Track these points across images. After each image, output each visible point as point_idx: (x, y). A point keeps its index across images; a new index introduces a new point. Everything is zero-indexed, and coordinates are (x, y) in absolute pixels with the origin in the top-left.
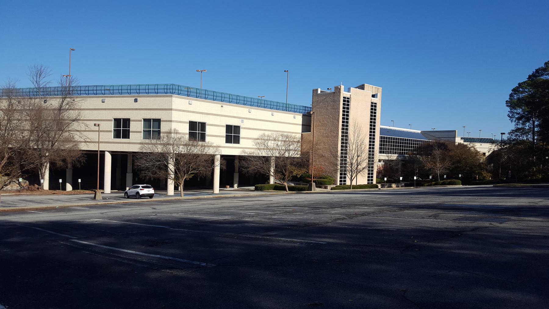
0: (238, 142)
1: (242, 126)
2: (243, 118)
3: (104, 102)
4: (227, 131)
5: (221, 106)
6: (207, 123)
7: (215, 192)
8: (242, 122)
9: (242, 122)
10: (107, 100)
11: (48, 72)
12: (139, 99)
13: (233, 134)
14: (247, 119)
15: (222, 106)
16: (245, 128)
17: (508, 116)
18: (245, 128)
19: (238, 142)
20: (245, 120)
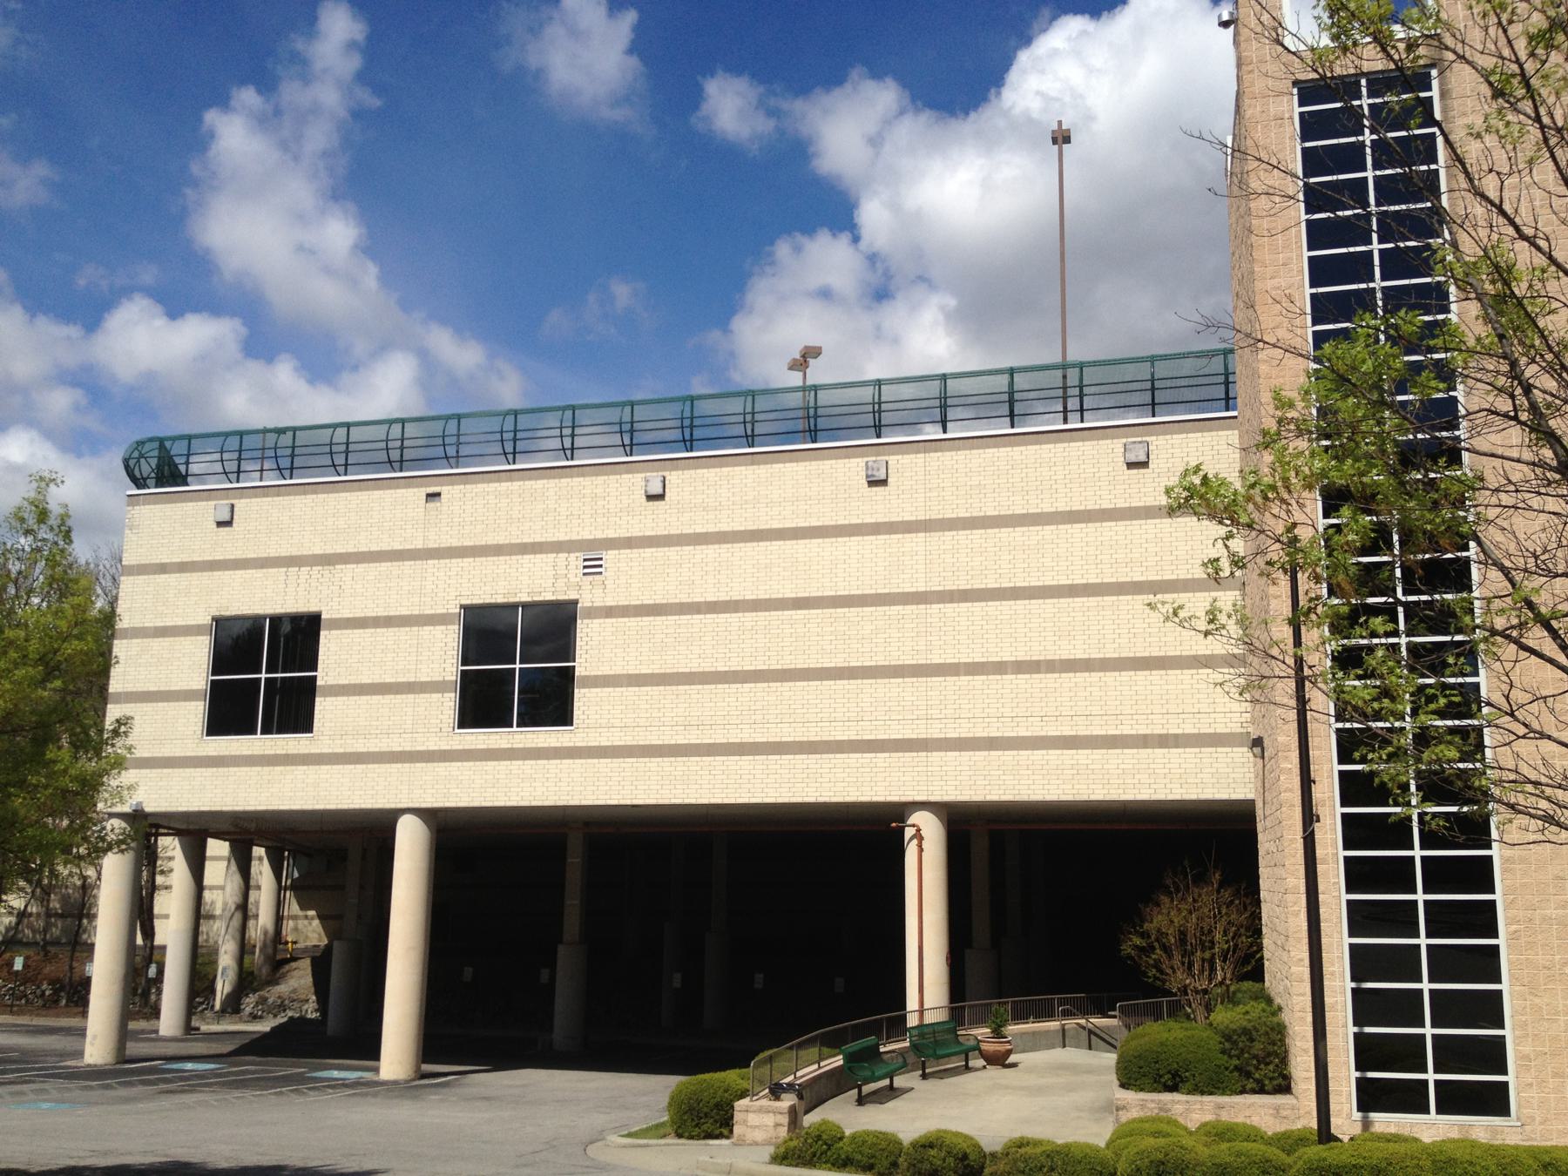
0: (560, 713)
1: (588, 595)
2: (592, 555)
3: (884, 482)
4: (221, 661)
5: (429, 495)
6: (584, 603)
7: (162, 1033)
8: (593, 566)
9: (593, 566)
10: (903, 466)
11: (1553, 142)
12: (445, 490)
13: (520, 669)
14: (629, 543)
15: (432, 496)
16: (609, 612)
17: (127, 467)
18: (609, 612)
19: (560, 713)
20: (610, 557)
